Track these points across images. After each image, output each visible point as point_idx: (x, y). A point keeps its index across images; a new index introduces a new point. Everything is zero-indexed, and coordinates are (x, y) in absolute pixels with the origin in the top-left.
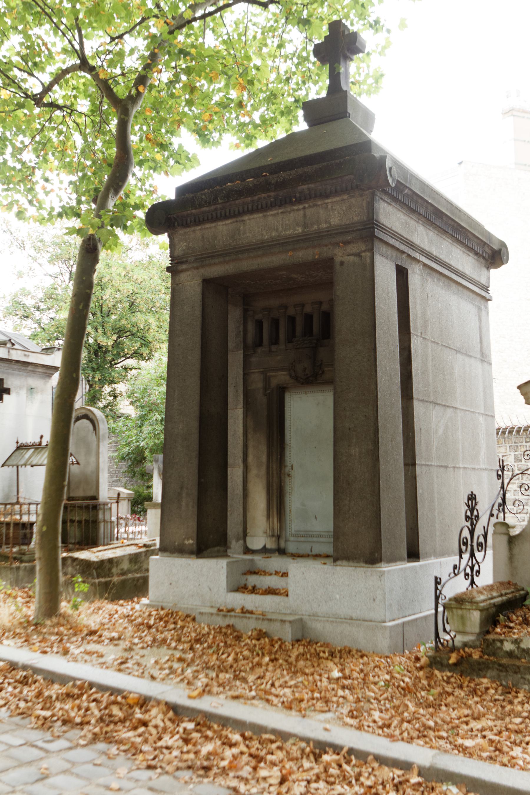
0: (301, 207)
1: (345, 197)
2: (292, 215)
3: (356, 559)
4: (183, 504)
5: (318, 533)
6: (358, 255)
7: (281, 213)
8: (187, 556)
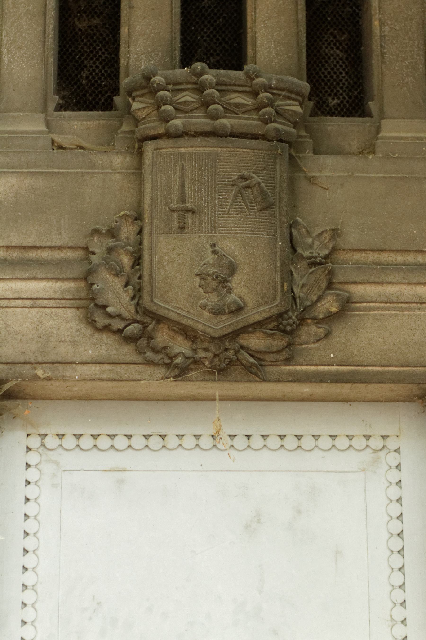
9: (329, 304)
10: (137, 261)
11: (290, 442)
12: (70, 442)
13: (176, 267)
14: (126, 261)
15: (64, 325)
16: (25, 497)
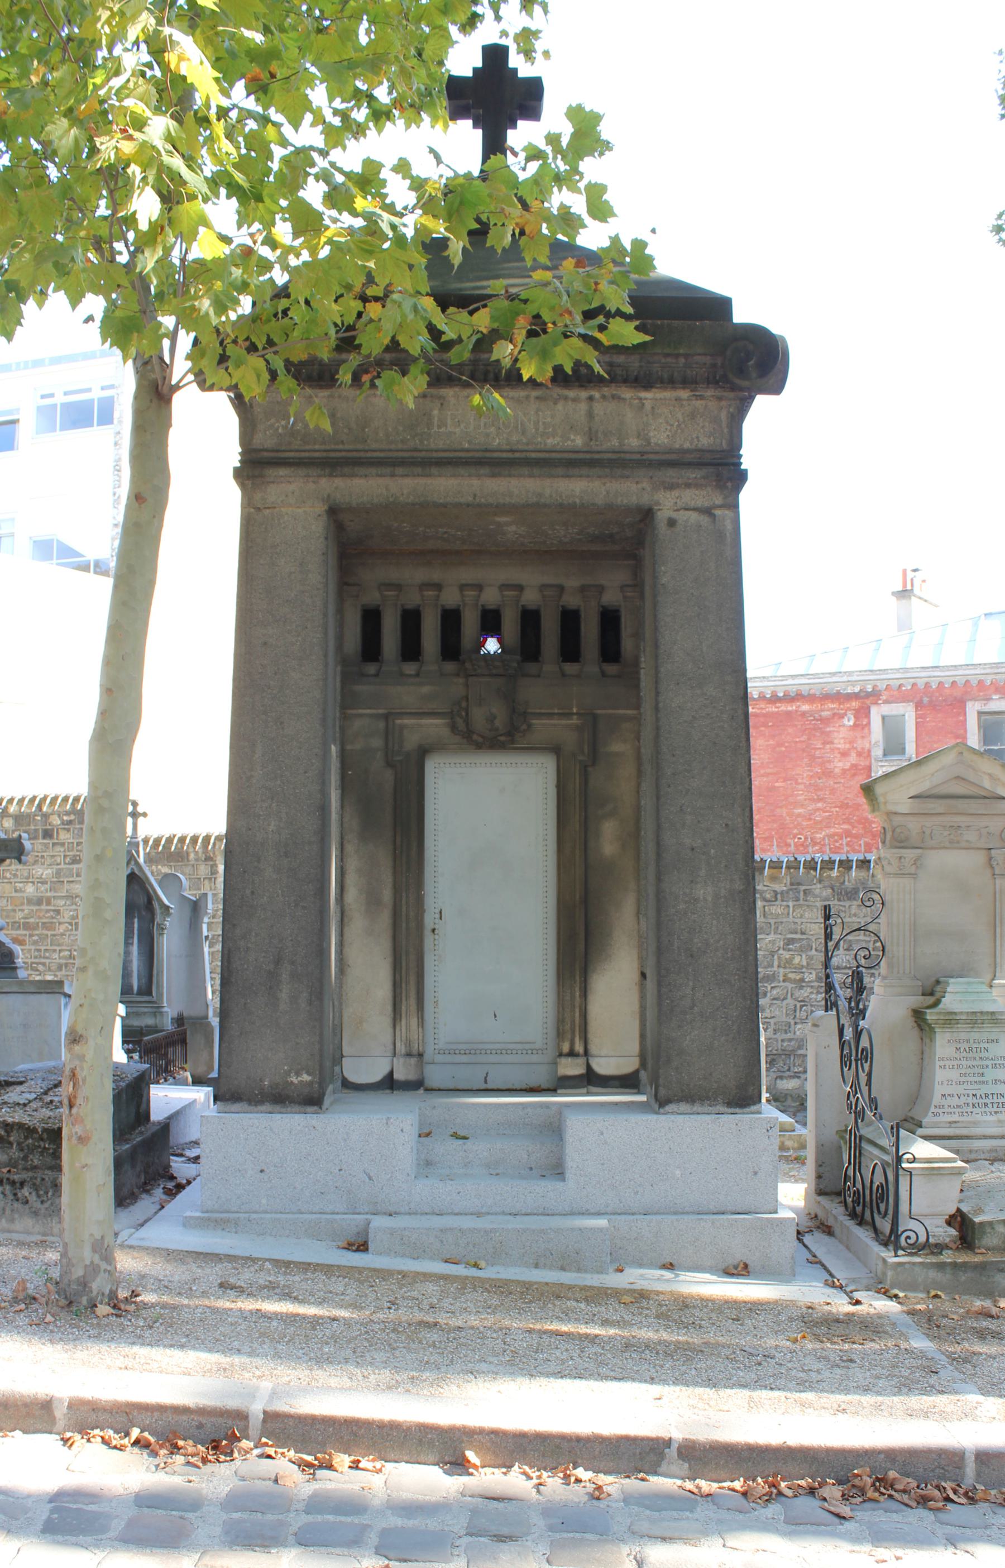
0: (584, 394)
1: (684, 394)
2: (560, 406)
3: (708, 1098)
4: (284, 995)
5: (498, 1046)
6: (708, 511)
7: (537, 398)
8: (297, 1108)
9: (524, 727)
10: (467, 714)
11: (514, 765)
12: (447, 765)
13: (478, 716)
14: (464, 714)
15: (445, 732)
16: (893, 594)
